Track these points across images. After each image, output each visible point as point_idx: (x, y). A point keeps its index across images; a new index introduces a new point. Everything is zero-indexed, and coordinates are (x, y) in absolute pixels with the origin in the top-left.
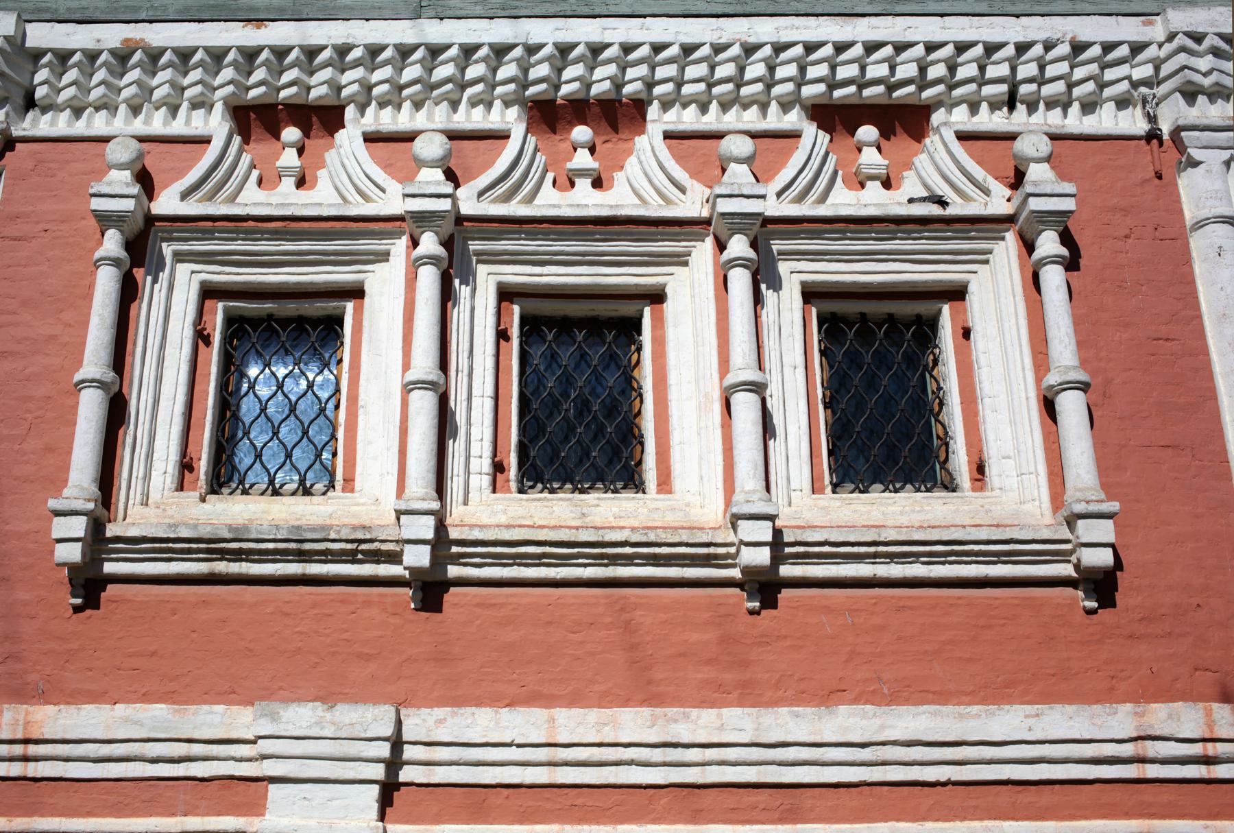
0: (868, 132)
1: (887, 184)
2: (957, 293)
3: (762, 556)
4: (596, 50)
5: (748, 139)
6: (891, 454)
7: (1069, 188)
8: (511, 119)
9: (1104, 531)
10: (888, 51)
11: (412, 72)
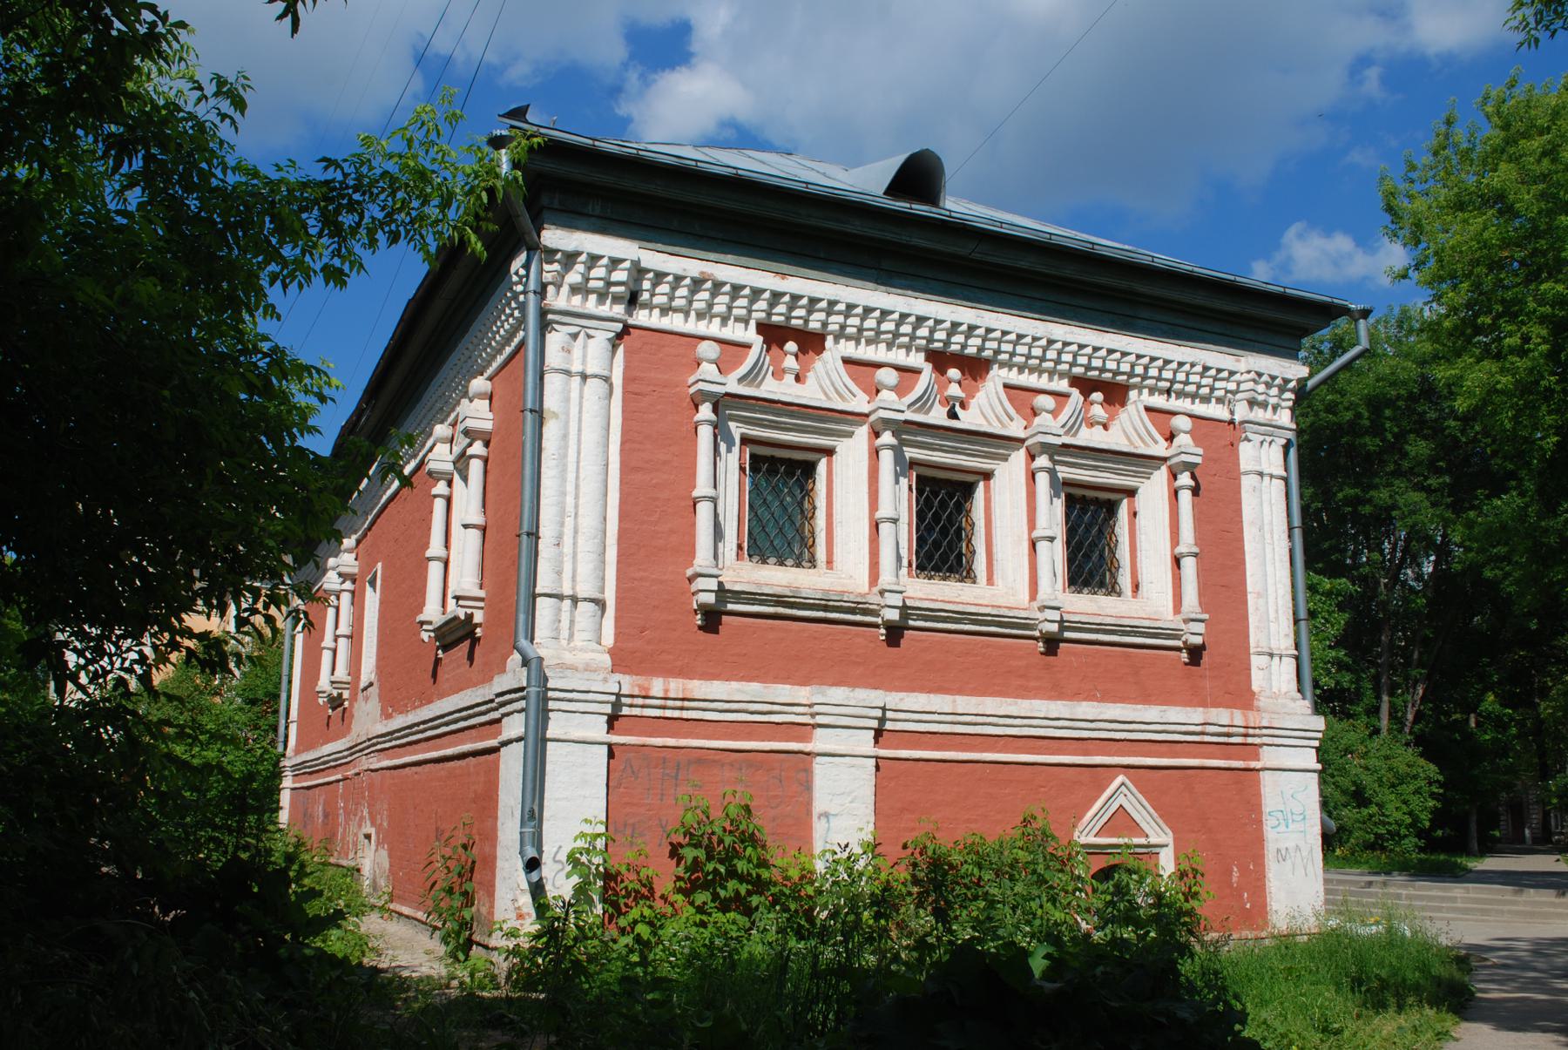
0: (1097, 396)
1: (1105, 427)
2: (829, 452)
3: (1054, 627)
4: (972, 328)
5: (894, 373)
6: (944, 559)
7: (1200, 451)
8: (751, 335)
9: (1200, 628)
10: (1118, 355)
11: (870, 323)
